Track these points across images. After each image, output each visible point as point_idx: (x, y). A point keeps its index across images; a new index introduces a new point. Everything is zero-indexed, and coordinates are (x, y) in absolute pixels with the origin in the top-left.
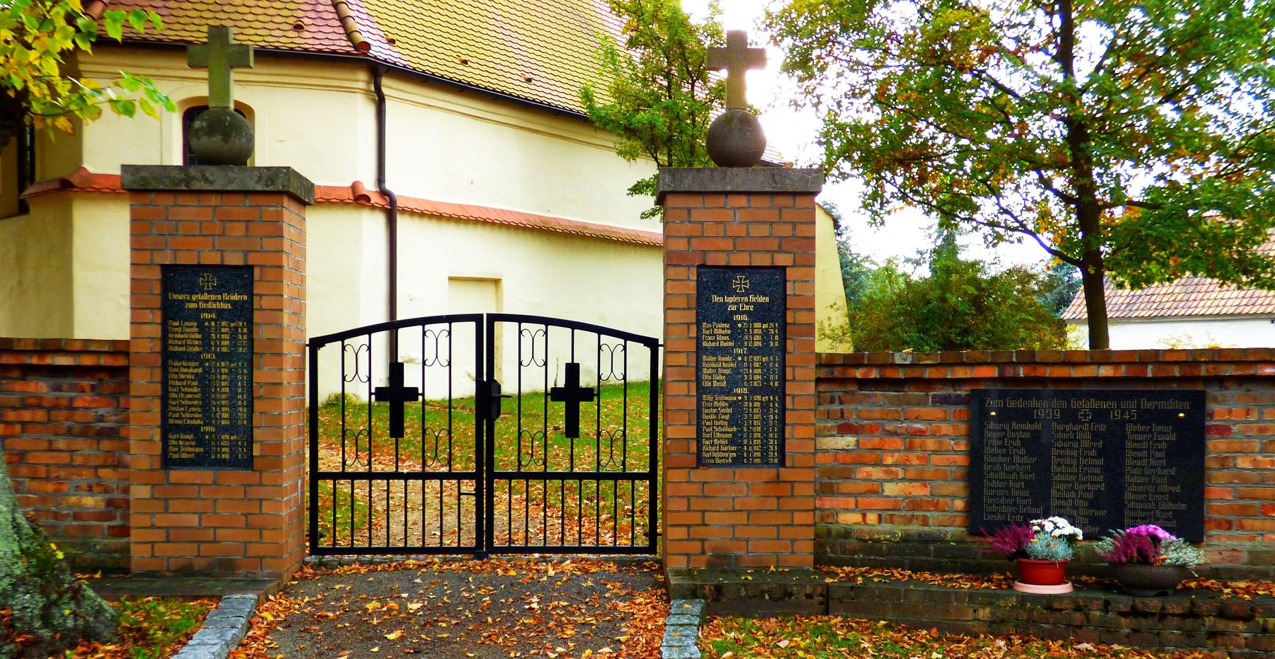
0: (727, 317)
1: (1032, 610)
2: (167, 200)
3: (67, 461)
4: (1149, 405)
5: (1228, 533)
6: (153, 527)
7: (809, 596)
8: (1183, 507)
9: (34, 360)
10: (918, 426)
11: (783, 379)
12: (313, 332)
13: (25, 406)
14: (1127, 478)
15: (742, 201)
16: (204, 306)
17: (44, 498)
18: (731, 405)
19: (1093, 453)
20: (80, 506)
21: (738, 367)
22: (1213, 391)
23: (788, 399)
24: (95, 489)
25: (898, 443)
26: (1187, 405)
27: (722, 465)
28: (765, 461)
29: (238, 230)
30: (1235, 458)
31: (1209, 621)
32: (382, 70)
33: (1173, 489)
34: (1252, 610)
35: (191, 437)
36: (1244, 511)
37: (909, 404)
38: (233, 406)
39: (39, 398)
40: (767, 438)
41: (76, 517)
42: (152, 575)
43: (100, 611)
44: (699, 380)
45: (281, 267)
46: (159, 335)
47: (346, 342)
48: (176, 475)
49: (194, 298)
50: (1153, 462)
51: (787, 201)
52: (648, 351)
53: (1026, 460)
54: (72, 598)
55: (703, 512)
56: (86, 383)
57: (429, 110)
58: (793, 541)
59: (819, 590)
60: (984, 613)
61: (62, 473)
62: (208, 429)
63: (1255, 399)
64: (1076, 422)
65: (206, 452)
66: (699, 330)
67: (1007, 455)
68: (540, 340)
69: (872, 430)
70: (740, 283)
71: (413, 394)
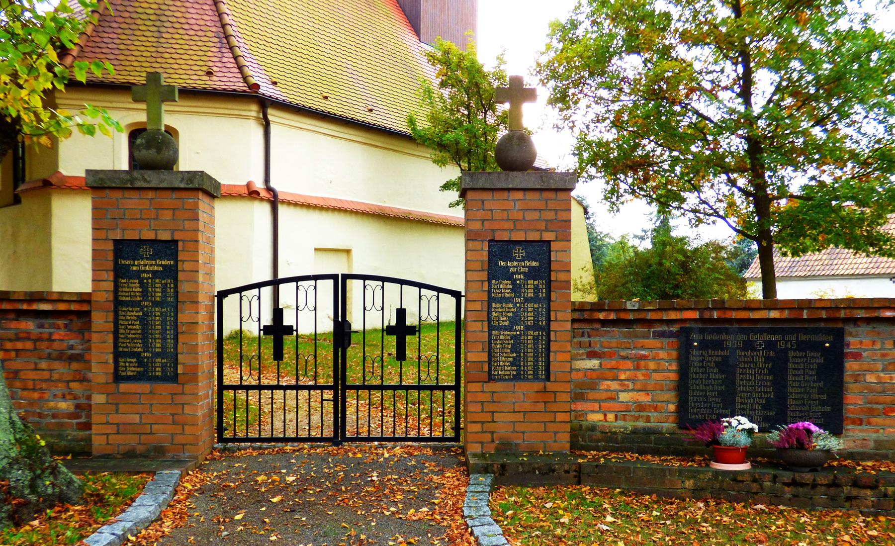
0: (509, 276)
1: (723, 481)
2: (118, 194)
3: (47, 377)
4: (803, 338)
5: (860, 427)
6: (108, 423)
7: (567, 472)
8: (828, 409)
9: (25, 307)
10: (643, 352)
11: (549, 320)
12: (220, 287)
13: (18, 339)
14: (789, 389)
15: (519, 195)
16: (144, 268)
17: (32, 403)
18: (512, 337)
19: (766, 371)
20: (56, 408)
21: (517, 312)
22: (849, 328)
23: (552, 334)
24: (67, 397)
25: (629, 364)
26: (831, 338)
27: (506, 380)
28: (536, 378)
29: (167, 215)
30: (865, 375)
31: (846, 489)
32: (268, 103)
33: (821, 397)
34: (877, 481)
35: (134, 360)
36: (871, 412)
37: (636, 337)
38: (164, 339)
39: (28, 333)
40: (537, 361)
41: (54, 416)
42: (107, 457)
43: (70, 482)
44: (489, 320)
45: (197, 241)
46: (112, 289)
47: (243, 293)
48: (124, 387)
49: (137, 263)
50: (807, 378)
51: (552, 195)
52: (454, 300)
53: (718, 376)
54: (51, 473)
55: (493, 413)
56: (61, 322)
57: (301, 132)
58: (555, 433)
59: (574, 467)
60: (689, 484)
61: (44, 386)
62: (146, 354)
63: (879, 334)
64: (754, 349)
65: (145, 371)
66: (490, 285)
67: (705, 373)
68: (379, 292)
69: (611, 355)
70: (519, 252)
71: (290, 330)
